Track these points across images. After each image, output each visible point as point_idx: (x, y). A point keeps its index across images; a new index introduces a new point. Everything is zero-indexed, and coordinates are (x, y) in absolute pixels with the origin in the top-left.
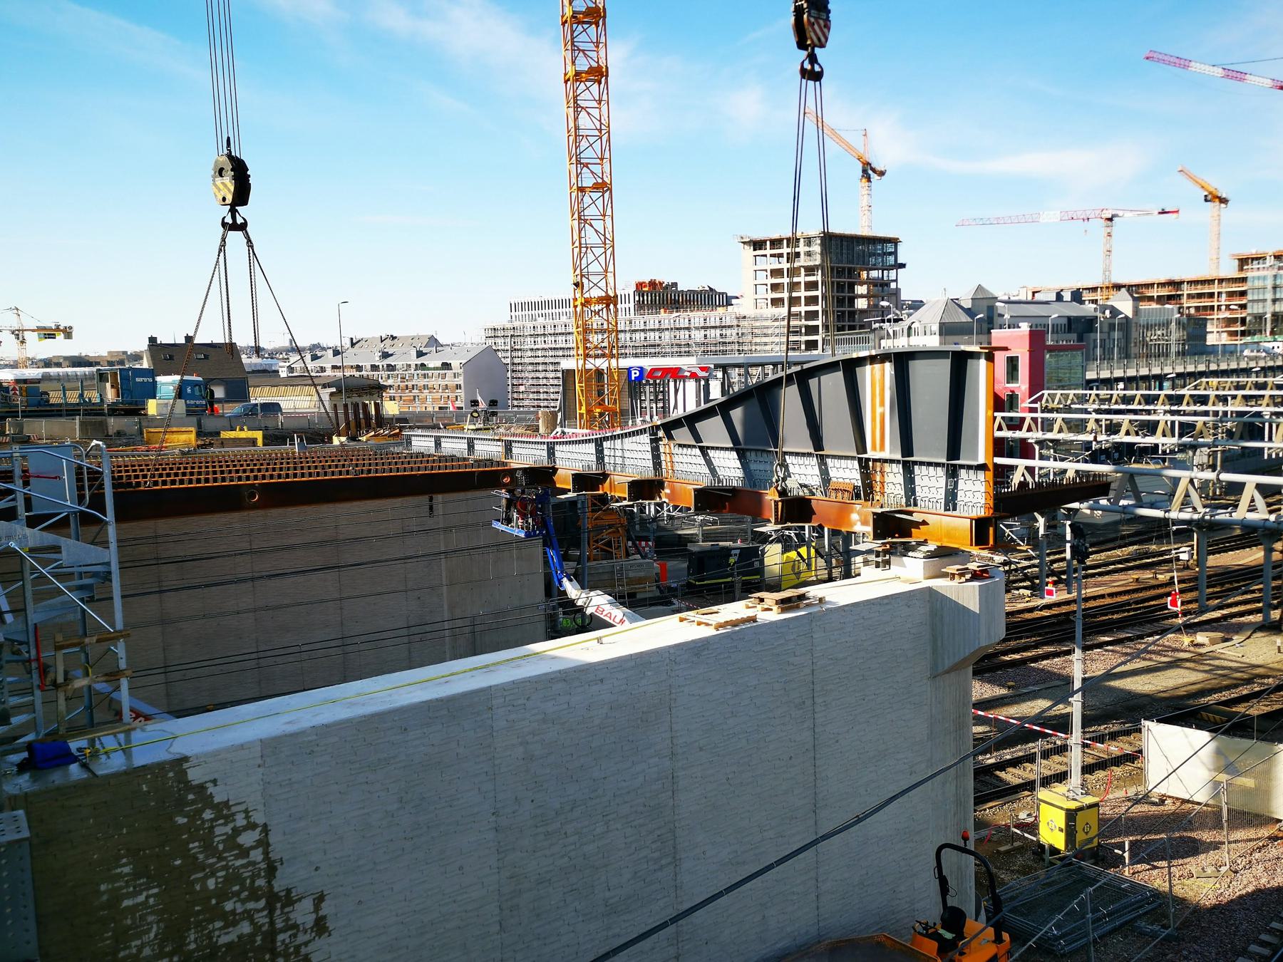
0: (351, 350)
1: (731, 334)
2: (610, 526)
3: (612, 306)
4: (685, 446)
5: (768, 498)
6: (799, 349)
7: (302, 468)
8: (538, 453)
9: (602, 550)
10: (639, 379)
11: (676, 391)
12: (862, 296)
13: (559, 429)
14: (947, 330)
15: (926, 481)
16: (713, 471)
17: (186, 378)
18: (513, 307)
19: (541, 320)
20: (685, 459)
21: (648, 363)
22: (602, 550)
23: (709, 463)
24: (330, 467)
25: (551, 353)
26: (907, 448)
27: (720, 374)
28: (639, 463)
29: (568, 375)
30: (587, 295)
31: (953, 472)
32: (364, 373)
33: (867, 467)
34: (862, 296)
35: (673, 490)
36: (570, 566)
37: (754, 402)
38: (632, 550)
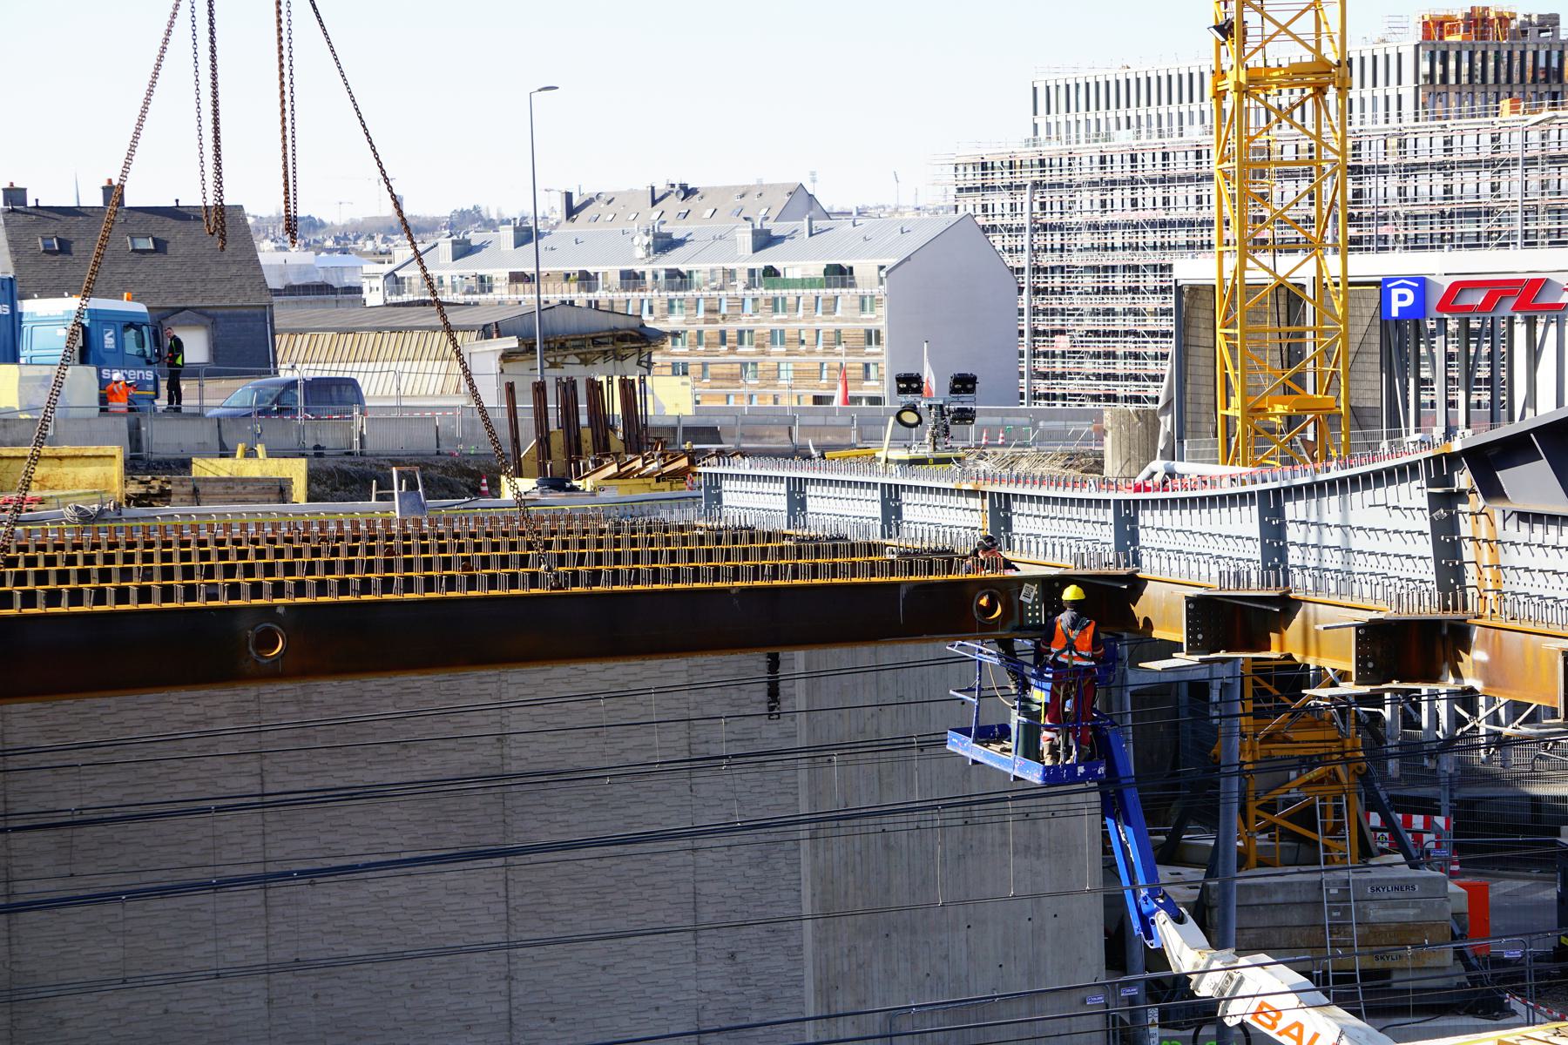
0: (567, 228)
2: (1308, 763)
3: (1331, 94)
4: (1538, 518)
7: (408, 565)
8: (1089, 532)
9: (1286, 834)
10: (1415, 314)
11: (1534, 354)
13: (1159, 465)
17: (97, 303)
18: (1043, 98)
19: (1124, 139)
20: (1539, 560)
22: (1286, 834)
24: (485, 562)
25: (1151, 238)
28: (1396, 568)
29: (1191, 303)
30: (1256, 61)
32: (600, 295)
35: (1497, 654)
36: (1183, 881)
38: (1383, 840)
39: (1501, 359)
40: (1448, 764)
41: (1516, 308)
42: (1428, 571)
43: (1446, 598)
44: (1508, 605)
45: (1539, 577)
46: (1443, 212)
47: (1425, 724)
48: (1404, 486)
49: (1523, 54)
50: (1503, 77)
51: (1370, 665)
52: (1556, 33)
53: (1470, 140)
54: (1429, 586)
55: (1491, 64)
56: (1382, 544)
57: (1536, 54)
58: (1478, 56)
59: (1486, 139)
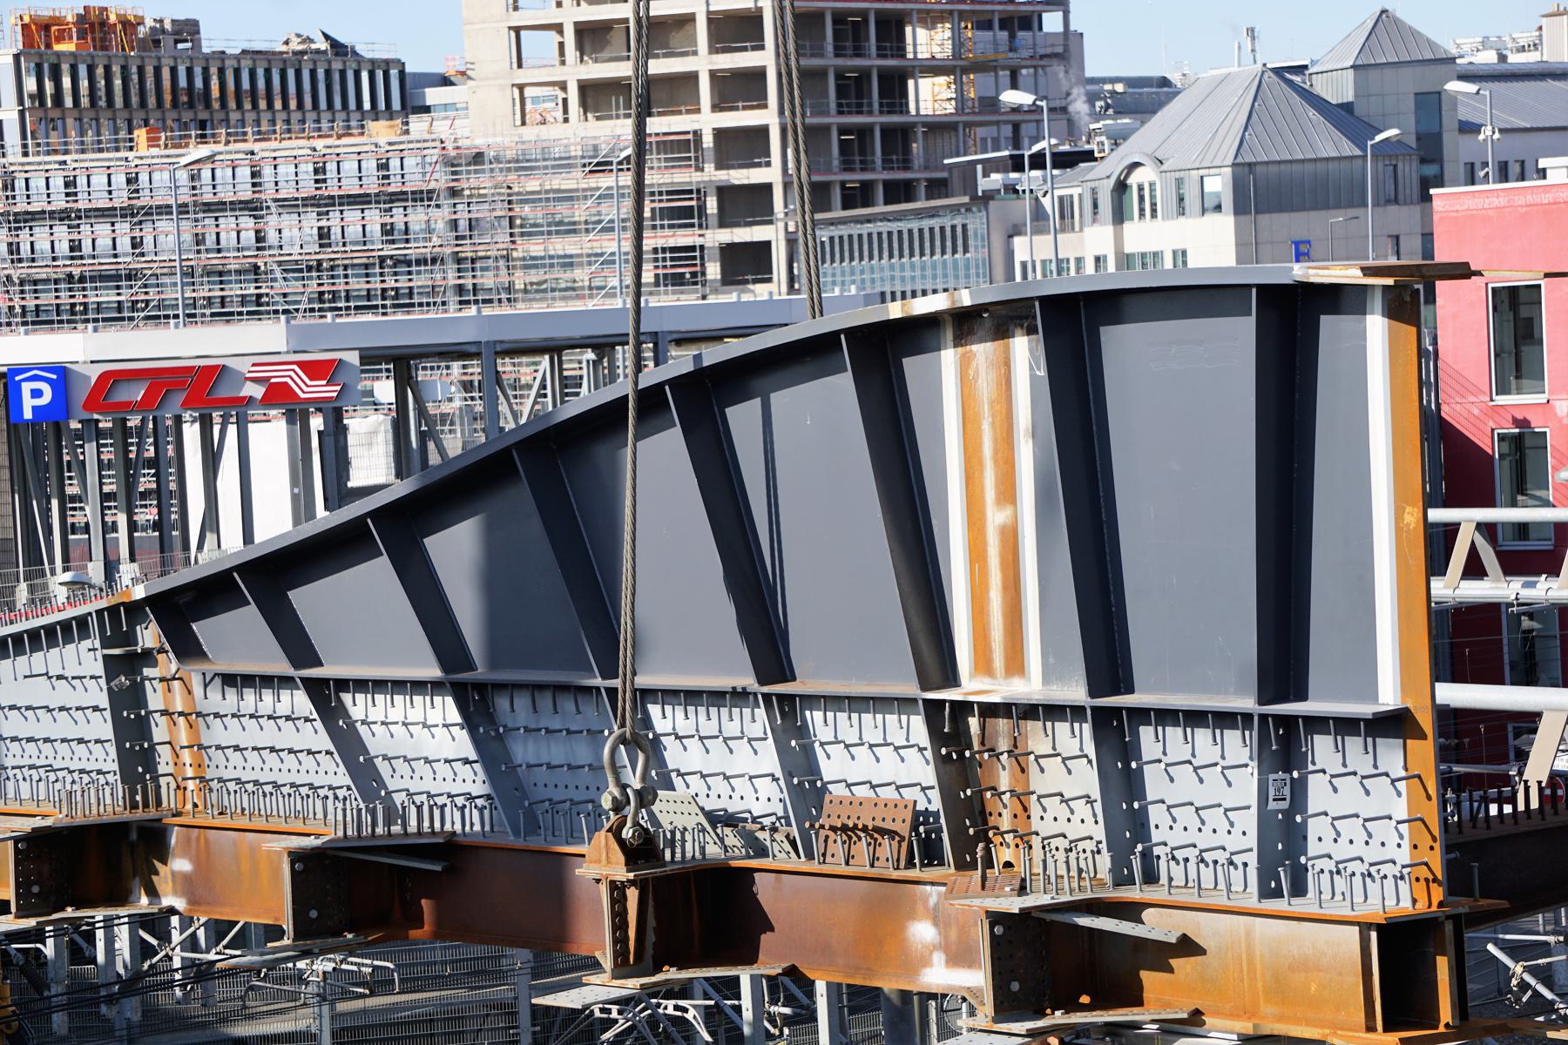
1: (429, 225)
5: (585, 872)
6: (698, 278)
10: (53, 420)
12: (934, 68)
14: (1260, 192)
15: (1185, 786)
16: (137, 756)
20: (252, 734)
21: (81, 349)
23: (348, 744)
26: (1108, 658)
27: (385, 390)
28: (63, 757)
31: (1284, 747)
33: (959, 738)
34: (934, 68)
35: (204, 862)
37: (520, 498)
39: (167, 465)
40: (132, 1009)
41: (187, 405)
42: (106, 758)
43: (133, 793)
44: (214, 795)
45: (253, 757)
46: (70, 276)
47: (101, 958)
48: (71, 647)
49: (158, 71)
50: (135, 100)
51: (36, 889)
52: (197, 44)
53: (99, 180)
54: (110, 778)
55: (118, 82)
56: (43, 726)
57: (174, 71)
58: (100, 71)
59: (119, 179)
